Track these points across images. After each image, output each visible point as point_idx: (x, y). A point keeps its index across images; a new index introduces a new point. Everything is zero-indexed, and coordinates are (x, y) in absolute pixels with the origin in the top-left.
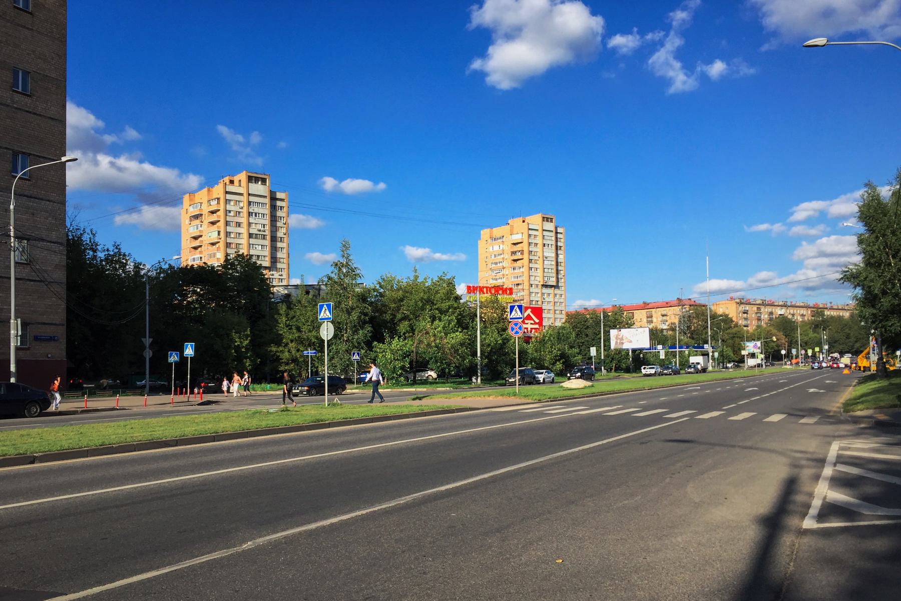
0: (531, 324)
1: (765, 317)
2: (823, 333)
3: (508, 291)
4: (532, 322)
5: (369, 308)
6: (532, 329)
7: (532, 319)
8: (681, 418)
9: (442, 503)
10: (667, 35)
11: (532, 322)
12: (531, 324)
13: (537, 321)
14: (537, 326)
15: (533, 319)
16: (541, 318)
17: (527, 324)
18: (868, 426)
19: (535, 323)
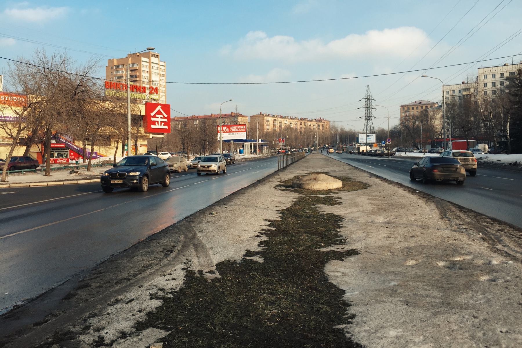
0: (161, 118)
1: (277, 124)
2: (316, 136)
3: (142, 90)
4: (162, 116)
5: (519, 311)
6: (161, 122)
7: (162, 114)
8: (6, 192)
9: (491, 114)
10: (413, 126)
11: (162, 116)
12: (161, 118)
13: (166, 116)
14: (166, 120)
15: (162, 114)
16: (168, 112)
17: (158, 118)
18: (24, 115)
19: (164, 118)
